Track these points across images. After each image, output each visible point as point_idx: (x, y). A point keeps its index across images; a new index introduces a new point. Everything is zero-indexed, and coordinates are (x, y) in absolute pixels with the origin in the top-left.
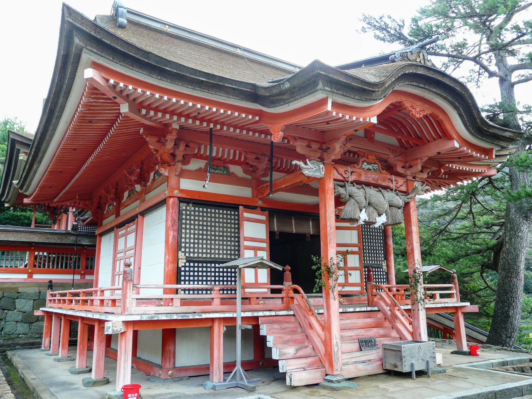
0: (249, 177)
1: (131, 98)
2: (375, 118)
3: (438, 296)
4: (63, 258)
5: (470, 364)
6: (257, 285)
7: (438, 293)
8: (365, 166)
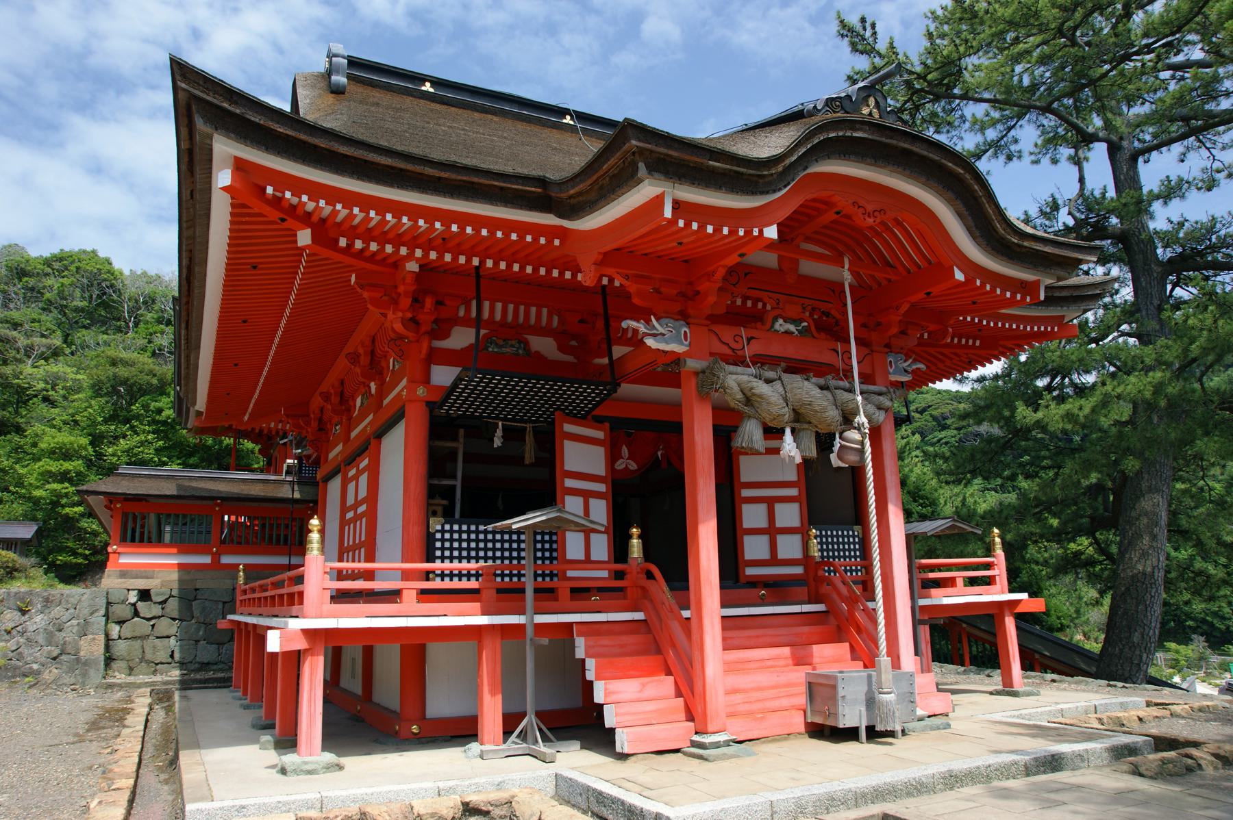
0: (570, 358)
1: (315, 219)
2: (774, 227)
3: (960, 582)
4: (271, 525)
5: (1009, 714)
6: (588, 562)
7: (960, 575)
8: (781, 326)
